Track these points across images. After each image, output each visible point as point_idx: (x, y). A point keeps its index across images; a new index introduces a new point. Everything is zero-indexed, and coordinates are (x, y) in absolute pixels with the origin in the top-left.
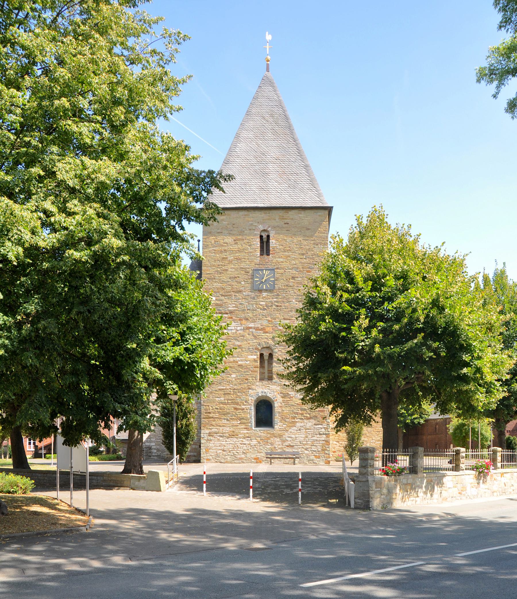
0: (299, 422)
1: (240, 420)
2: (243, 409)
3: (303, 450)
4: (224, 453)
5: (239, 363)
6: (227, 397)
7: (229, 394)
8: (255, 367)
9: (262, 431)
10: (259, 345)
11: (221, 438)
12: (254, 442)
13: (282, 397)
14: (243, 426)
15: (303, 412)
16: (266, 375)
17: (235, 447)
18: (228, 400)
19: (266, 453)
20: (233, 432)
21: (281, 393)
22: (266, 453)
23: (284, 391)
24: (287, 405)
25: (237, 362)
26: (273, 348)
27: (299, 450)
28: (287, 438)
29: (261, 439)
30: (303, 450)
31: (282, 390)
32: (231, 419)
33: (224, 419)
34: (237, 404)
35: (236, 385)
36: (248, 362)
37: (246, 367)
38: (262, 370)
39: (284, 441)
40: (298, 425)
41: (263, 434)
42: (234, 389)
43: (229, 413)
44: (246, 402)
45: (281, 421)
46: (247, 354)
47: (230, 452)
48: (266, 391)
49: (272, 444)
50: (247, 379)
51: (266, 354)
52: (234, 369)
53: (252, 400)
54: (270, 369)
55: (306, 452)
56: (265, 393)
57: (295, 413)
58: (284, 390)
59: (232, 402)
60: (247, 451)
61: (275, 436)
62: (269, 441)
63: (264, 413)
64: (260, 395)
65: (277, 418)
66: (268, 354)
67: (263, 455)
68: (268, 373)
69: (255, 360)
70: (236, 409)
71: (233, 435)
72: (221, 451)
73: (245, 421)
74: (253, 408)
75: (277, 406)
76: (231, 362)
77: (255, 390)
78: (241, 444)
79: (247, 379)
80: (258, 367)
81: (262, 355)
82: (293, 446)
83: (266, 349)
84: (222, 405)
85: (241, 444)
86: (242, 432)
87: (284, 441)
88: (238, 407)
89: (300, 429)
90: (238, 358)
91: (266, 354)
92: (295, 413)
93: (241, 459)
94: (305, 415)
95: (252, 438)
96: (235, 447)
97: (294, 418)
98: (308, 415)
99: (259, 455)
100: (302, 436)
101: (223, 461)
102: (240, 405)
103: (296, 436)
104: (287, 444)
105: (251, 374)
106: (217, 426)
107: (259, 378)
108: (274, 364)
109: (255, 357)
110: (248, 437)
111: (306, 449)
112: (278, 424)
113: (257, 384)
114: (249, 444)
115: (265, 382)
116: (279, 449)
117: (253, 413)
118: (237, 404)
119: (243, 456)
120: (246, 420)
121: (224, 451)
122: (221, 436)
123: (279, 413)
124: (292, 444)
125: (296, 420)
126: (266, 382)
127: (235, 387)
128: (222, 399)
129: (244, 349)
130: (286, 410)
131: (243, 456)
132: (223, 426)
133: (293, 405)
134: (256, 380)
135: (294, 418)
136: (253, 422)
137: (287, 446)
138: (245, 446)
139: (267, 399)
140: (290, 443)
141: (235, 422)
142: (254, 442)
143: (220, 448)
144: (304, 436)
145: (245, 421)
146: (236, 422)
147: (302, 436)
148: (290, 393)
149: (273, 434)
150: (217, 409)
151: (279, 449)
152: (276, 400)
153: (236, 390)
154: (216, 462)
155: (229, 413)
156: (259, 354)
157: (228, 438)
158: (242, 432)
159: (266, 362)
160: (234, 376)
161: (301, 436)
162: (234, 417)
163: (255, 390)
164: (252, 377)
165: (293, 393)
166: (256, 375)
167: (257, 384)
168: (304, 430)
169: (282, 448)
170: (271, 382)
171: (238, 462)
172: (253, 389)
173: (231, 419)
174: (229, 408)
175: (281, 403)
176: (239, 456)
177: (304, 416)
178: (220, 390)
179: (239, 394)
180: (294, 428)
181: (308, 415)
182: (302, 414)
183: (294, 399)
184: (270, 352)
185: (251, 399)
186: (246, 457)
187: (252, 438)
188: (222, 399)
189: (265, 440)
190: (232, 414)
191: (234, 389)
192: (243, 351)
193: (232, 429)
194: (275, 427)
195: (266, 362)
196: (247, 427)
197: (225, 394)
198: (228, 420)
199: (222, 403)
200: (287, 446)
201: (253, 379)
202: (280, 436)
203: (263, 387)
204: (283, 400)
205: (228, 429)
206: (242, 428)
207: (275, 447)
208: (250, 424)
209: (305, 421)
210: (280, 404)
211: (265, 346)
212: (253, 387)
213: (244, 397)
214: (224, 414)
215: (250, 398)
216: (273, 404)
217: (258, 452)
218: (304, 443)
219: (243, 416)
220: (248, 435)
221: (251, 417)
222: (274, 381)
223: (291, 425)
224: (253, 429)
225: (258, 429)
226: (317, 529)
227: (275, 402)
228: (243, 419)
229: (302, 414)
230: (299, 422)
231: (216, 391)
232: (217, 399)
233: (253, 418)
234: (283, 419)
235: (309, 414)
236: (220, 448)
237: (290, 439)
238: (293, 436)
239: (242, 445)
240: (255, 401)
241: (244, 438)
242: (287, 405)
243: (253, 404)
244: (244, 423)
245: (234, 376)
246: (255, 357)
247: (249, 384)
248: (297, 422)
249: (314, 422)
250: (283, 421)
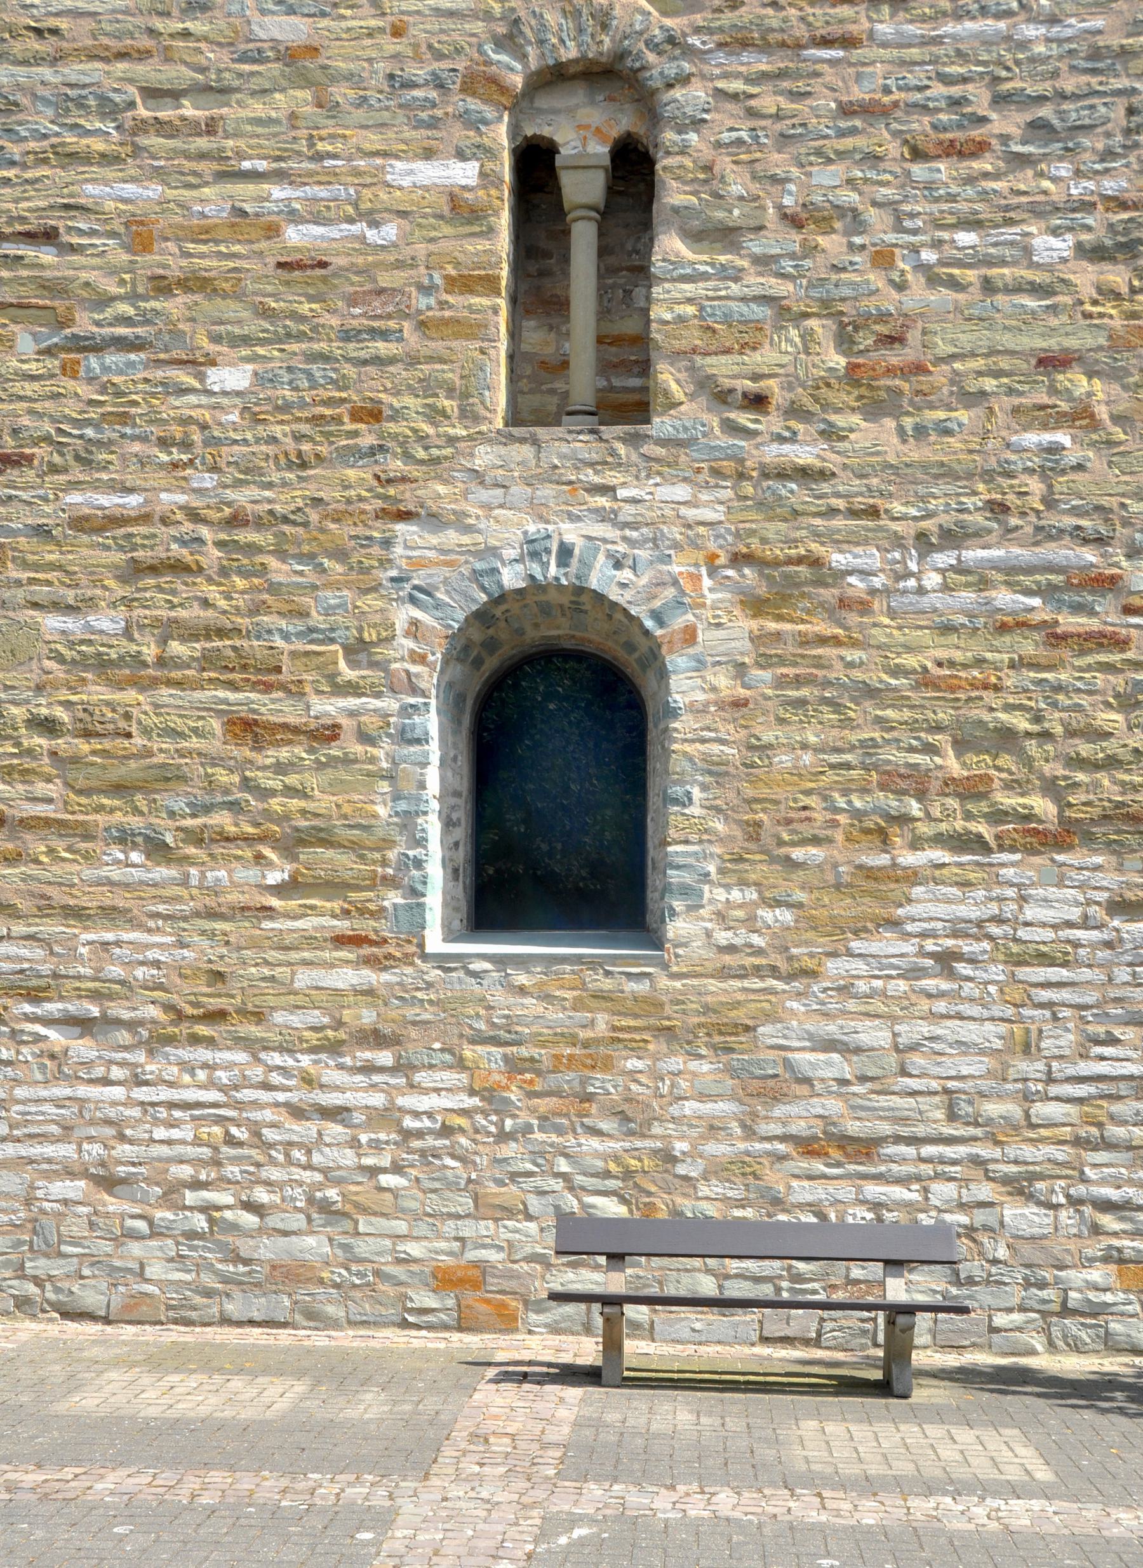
0: (934, 874)
1: (292, 844)
2: (329, 733)
3: (985, 1191)
4: (113, 1204)
5: (294, 235)
6: (158, 600)
7: (178, 567)
8: (463, 284)
9: (537, 979)
10: (510, 41)
11: (83, 1048)
12: (438, 1095)
13: (756, 606)
14: (323, 918)
15: (980, 763)
16: (583, 382)
17: (236, 1139)
18: (168, 630)
19: (564, 1219)
20: (219, 976)
21: (738, 559)
22: (564, 1219)
23: (773, 537)
24: (807, 686)
25: (272, 231)
26: (658, 66)
27: (943, 1191)
28: (804, 1059)
29: (514, 1066)
30: (985, 1191)
31: (755, 520)
32: (196, 838)
33: (125, 838)
34: (266, 675)
35: (250, 472)
36: (390, 231)
37: (371, 286)
38: (535, 337)
39: (769, 1087)
40: (927, 906)
41: (531, 1006)
42: (236, 521)
43: (169, 777)
44: (357, 650)
45: (735, 866)
46: (373, 140)
47: (171, 1194)
48: (572, 533)
49: (631, 1118)
50: (372, 414)
51: (583, 137)
52: (232, 309)
53: (419, 641)
54: (629, 326)
55: (1021, 1216)
56: (565, 553)
57: (890, 780)
58: (774, 529)
59: (208, 660)
60: (361, 1189)
61: (667, 1033)
62: (602, 1083)
63: (559, 781)
64: (511, 578)
65: (691, 831)
66: (600, 150)
67: (534, 1235)
68: (605, 367)
69: (462, 210)
70: (247, 728)
71: (206, 1015)
72: (76, 1188)
73: (343, 862)
74: (432, 723)
75: (688, 691)
76: (205, 233)
77: (460, 522)
78: (297, 1112)
79: (372, 414)
80: (490, 284)
81: (535, 165)
82: (863, 1148)
83: (575, 97)
84: (98, 693)
85: (297, 1112)
86: (304, 978)
87: (769, 1087)
88: (271, 707)
89: (946, 960)
90: (278, 192)
91: (583, 137)
92: (890, 780)
93: (290, 1274)
94: (1008, 801)
95: (414, 1052)
96: (236, 1139)
97: (882, 837)
98: (1043, 806)
99: (492, 1243)
100: (970, 1032)
101: (91, 1297)
102: (295, 691)
103: (909, 1032)
104: (799, 1115)
105: (412, 361)
106: (46, 908)
107: (501, 399)
108: (670, 246)
109: (465, 173)
110: (377, 1038)
111: (1020, 1187)
112: (706, 902)
113: (484, 457)
114: (387, 1116)
115: (567, 446)
116: (717, 1170)
117: (434, 769)
118: (266, 675)
119: (313, 1245)
120: (354, 846)
121: (109, 1183)
122: (82, 1025)
123: (717, 771)
124: (853, 1128)
125: (909, 859)
126: (583, 446)
127: (241, 497)
128: (107, 622)
129: (341, 93)
130: (798, 747)
131: (313, 1245)
132: (111, 914)
133: (870, 692)
134: (468, 415)
135: (882, 837)
136: (435, 871)
137: (808, 1146)
138: (334, 1130)
139: (594, 636)
140: (833, 1106)
141: (235, 877)
142: (438, 1095)
143: (65, 1151)
144: (991, 1034)
145: (343, 862)
146: (248, 874)
147: (970, 1032)
148: (838, 559)
149: (652, 1004)
150: (48, 726)
151: (717, 1170)
152: (690, 635)
153: (259, 524)
154: (23, 1303)
155: (169, 777)
156: (501, 135)
157: (157, 1042)
158: (304, 978)
159: (584, 239)
160: (231, 377)
161: (965, 1039)
162: (222, 819)
163: (460, 522)
164: (427, 388)
165: (872, 558)
166: (474, 374)
167: (484, 457)
168: (997, 972)
169: (742, 1169)
170: (634, 440)
171: (258, 1307)
172: (435, 520)
173: (196, 838)
174: (183, 718)
175: (740, 669)
176: (267, 1249)
177: (998, 816)
178: (81, 523)
179: (280, 570)
180: (886, 944)
181: (1043, 806)
182: (971, 790)
183: (882, 627)
184: (625, 122)
185: (414, 629)
186: (351, 1258)
187: (414, 1052)
188: (107, 622)
189: (560, 1080)
190: (210, 784)
191: (236, 521)
192: (332, 109)
193: (200, 951)
194: (677, 928)
195: (584, 239)
196: (366, 926)
197: (136, 570)
198: (157, 849)
199: (102, 664)
200: (808, 1146)
201: (435, 415)
202: (726, 1032)
203: (547, 491)
204: (757, 639)
205: (158, 943)
206: (309, 940)
207: (669, 1158)
208: (394, 898)
209: (1011, 865)
210: (723, 681)
211: (570, 52)
212: (439, 492)
213: (332, 602)
214: (119, 789)
215: (403, 615)
216: (648, 685)
217: (484, 1208)
218: (992, 1109)
219: (323, 802)
220: (368, 1017)
221: (408, 821)
222: (661, 425)
223: (843, 908)
224: (435, 942)
225: (484, 948)
226: (336, 949)
227: (677, 661)
228: (323, 838)
229: (971, 790)
230: (934, 874)
231: (42, 532)
232: (52, 622)
233: (432, 826)
234: (759, 845)
235: (1051, 788)
236: (65, 1151)
237: (835, 1065)
238: (874, 1035)
239: (307, 1130)
240: (464, 649)
241: (334, 1048)
242: (807, 686)
243: (429, 679)
244: (333, 887)
245: (231, 377)
246: (465, 173)
247: (396, 466)
248: (913, 877)
249: (1110, 880)
250: (760, 870)
